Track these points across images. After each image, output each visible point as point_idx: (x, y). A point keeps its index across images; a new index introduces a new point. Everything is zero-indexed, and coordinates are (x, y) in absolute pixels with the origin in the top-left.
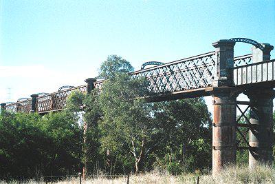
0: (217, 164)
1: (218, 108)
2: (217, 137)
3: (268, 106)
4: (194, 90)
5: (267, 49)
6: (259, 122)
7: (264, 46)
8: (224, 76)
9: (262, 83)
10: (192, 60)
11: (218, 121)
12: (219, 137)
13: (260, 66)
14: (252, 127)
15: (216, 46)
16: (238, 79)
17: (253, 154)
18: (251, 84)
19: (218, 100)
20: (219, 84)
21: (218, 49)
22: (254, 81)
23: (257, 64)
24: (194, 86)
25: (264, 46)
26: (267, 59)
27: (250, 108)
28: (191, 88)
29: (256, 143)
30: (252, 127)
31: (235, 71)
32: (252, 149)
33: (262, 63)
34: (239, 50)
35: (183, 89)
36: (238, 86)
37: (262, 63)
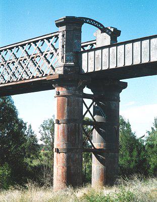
0: (60, 178)
1: (63, 103)
2: (61, 137)
3: (115, 100)
4: (26, 81)
5: (114, 34)
6: (107, 119)
7: (112, 30)
8: (70, 61)
9: (109, 70)
10: (11, 49)
11: (63, 116)
12: (64, 136)
13: (106, 50)
14: (96, 125)
15: (59, 25)
16: (89, 63)
17: (98, 158)
18: (102, 71)
19: (63, 91)
20: (65, 71)
21: (64, 28)
22: (113, 66)
23: (102, 48)
24: (25, 76)
25: (112, 30)
26: (114, 43)
27: (94, 103)
28: (9, 82)
29: (102, 144)
30: (96, 125)
31: (84, 56)
32: (97, 152)
33: (109, 47)
34: (88, 33)
35: (9, 82)
36: (88, 74)
37: (109, 47)
